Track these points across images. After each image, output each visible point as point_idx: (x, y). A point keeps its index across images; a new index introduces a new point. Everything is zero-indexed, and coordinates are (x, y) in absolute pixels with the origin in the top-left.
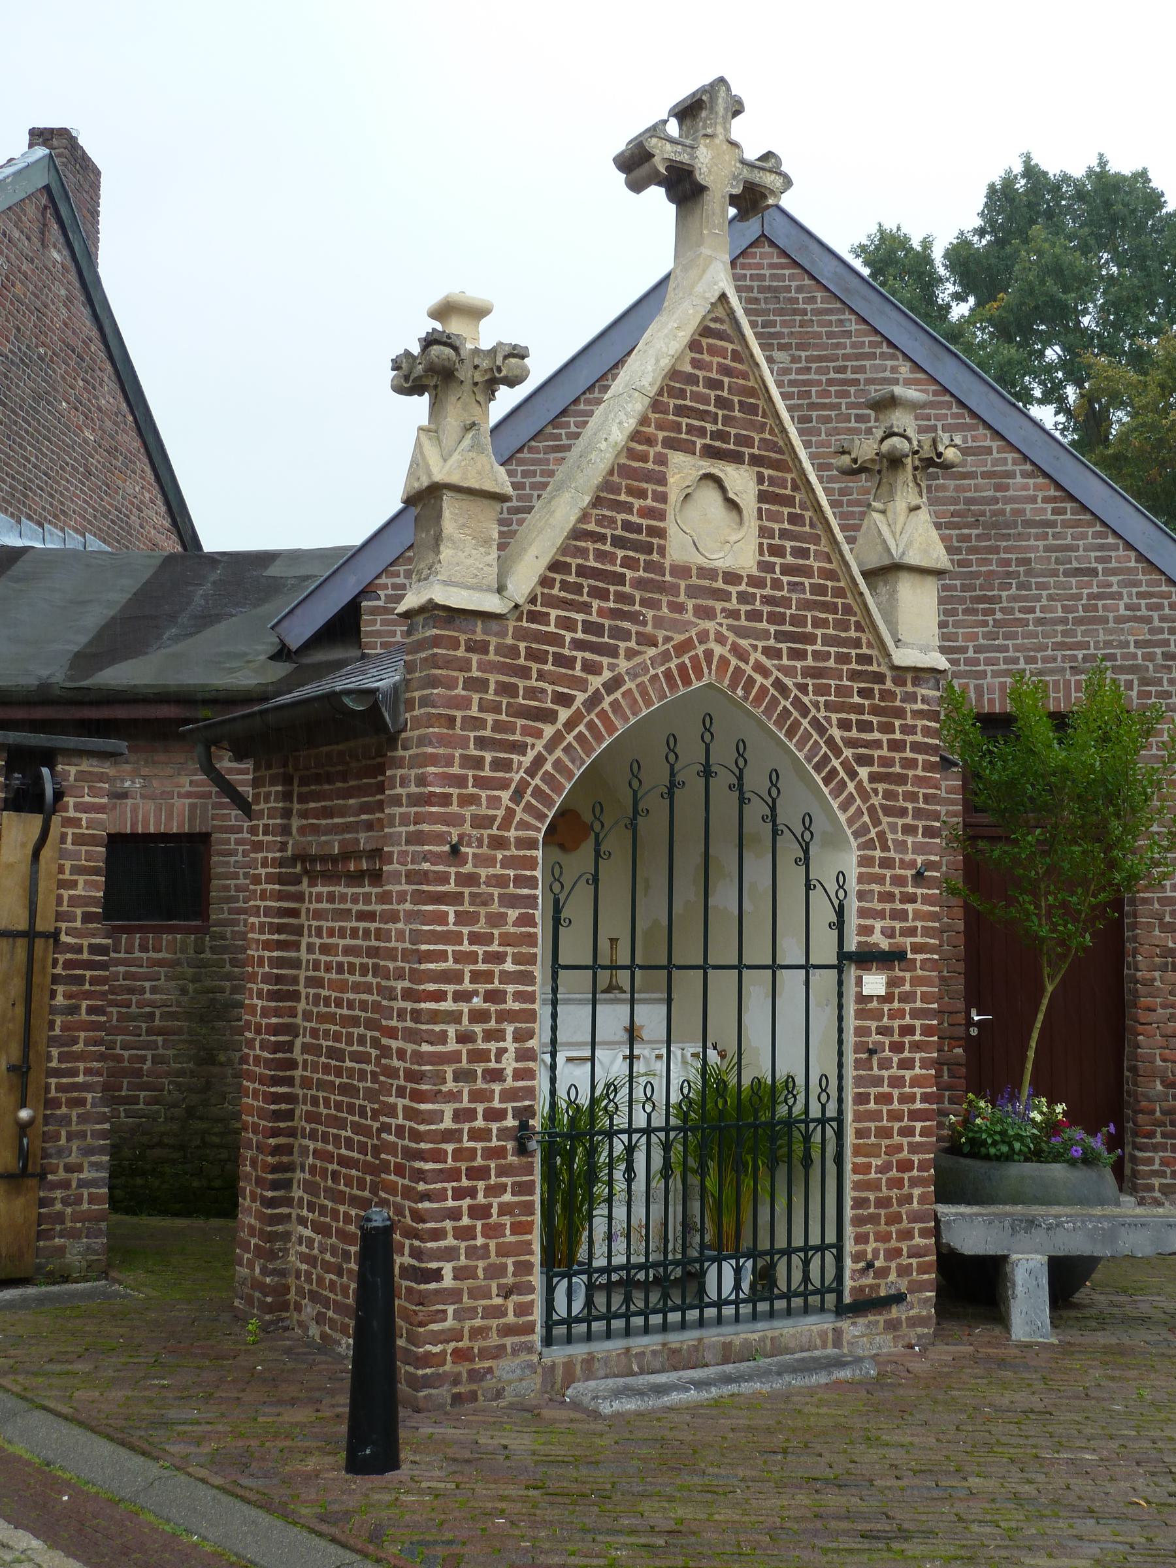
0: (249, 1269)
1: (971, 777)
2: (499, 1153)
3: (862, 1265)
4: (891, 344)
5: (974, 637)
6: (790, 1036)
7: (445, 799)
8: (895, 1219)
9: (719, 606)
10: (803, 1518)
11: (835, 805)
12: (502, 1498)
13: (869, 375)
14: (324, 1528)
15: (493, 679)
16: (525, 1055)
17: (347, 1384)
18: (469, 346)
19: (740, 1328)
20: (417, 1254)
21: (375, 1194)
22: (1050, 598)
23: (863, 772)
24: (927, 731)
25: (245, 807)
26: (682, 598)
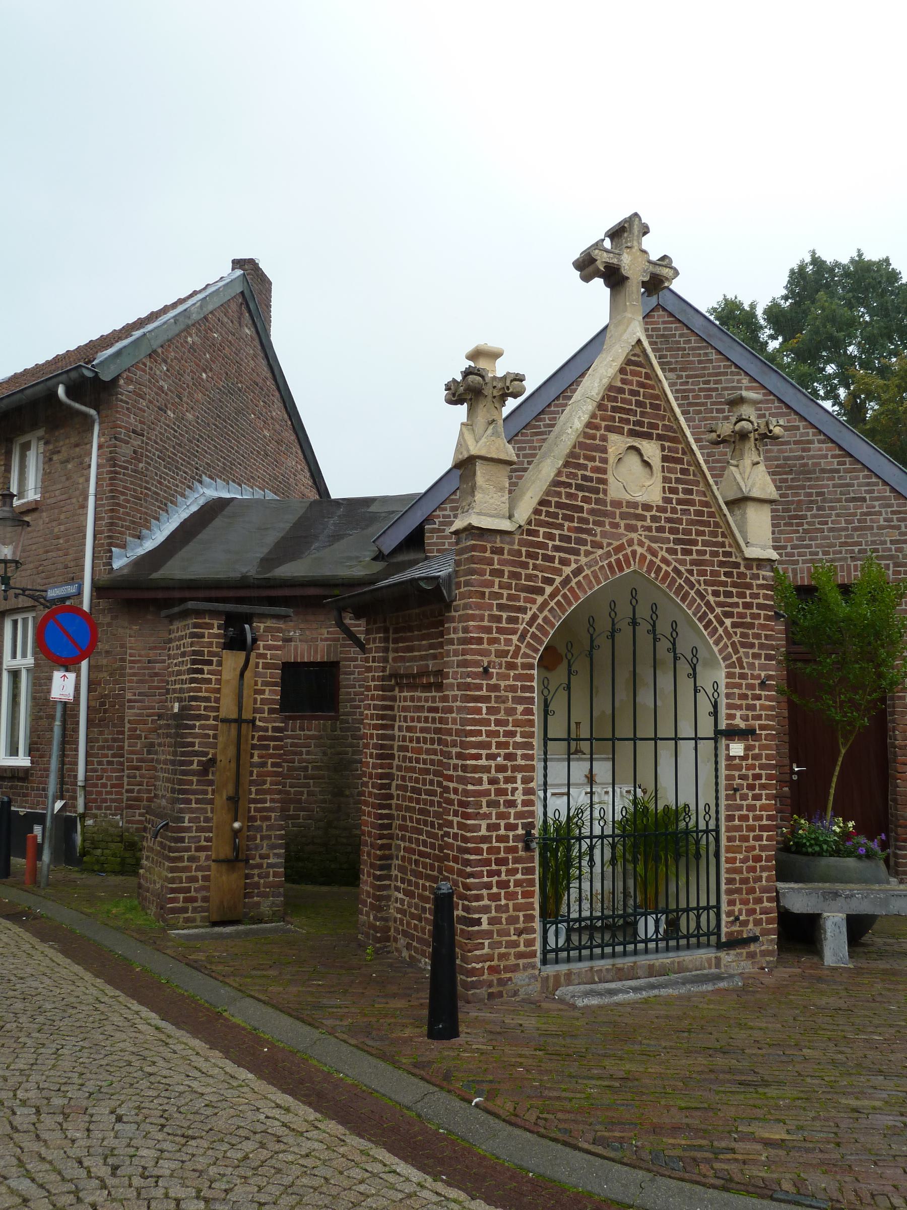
0: (367, 916)
1: (791, 624)
2: (514, 850)
3: (732, 918)
4: (737, 366)
5: (791, 540)
6: (686, 780)
7: (480, 641)
8: (752, 891)
9: (639, 524)
10: (702, 1072)
11: (711, 642)
12: (520, 1056)
13: (724, 385)
14: (416, 1071)
15: (507, 569)
16: (529, 792)
17: (427, 985)
18: (490, 375)
19: (659, 955)
20: (466, 909)
21: (440, 872)
22: (838, 515)
23: (728, 622)
24: (766, 597)
25: (362, 647)
26: (618, 520)
